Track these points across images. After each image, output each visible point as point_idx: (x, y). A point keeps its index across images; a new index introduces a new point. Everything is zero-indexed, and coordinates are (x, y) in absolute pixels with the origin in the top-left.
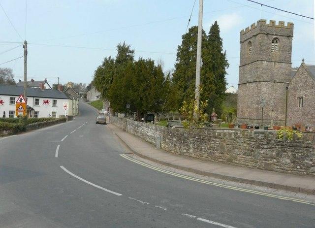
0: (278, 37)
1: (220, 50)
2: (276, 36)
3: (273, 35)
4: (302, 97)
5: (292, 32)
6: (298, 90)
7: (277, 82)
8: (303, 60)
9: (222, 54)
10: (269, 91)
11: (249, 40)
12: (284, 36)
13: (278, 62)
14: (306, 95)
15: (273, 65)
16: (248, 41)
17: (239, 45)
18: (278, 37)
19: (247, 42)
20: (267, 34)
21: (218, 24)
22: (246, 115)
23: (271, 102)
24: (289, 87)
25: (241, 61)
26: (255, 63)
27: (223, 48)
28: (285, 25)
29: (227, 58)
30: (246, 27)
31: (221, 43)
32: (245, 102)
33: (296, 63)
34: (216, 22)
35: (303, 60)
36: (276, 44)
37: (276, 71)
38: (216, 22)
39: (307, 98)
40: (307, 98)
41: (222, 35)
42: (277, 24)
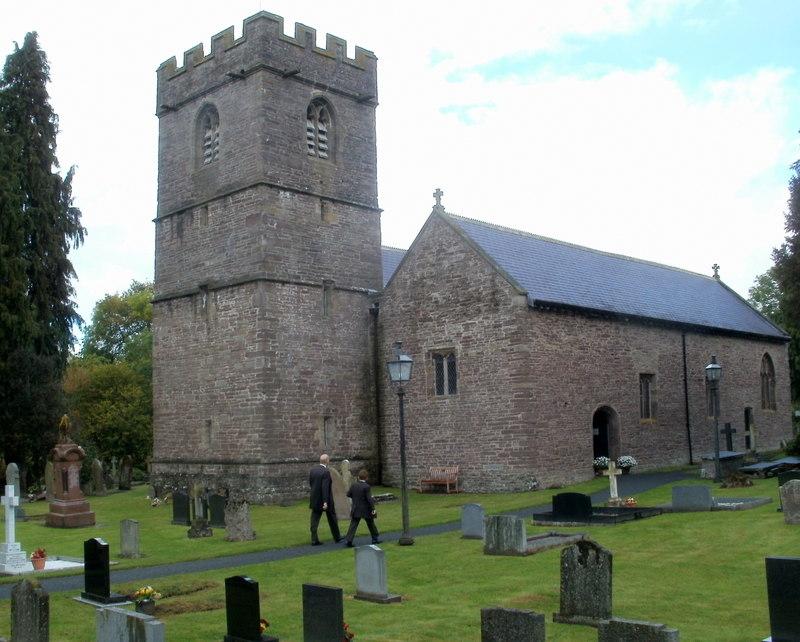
0: (328, 95)
1: (48, 159)
2: (316, 92)
3: (309, 83)
4: (452, 355)
5: (372, 84)
6: (426, 319)
7: (337, 289)
8: (438, 194)
9: (57, 178)
10: (307, 330)
11: (208, 99)
12: (347, 95)
13: (333, 201)
14: (467, 341)
15: (318, 211)
16: (200, 102)
17: (155, 122)
18: (328, 95)
19: (192, 111)
20: (291, 75)
21: (43, 44)
22: (203, 445)
23: (320, 375)
24: (384, 310)
25: (162, 192)
26: (241, 196)
27: (58, 154)
28: (81, 567)
29: (81, 197)
30: (189, 46)
31: (50, 132)
32: (196, 386)
33: (398, 230)
34: (31, 39)
35: (438, 194)
36: (321, 127)
37: (327, 235)
38: (31, 39)
39: (472, 352)
40: (472, 352)
41: (57, 94)
42: (321, 43)
